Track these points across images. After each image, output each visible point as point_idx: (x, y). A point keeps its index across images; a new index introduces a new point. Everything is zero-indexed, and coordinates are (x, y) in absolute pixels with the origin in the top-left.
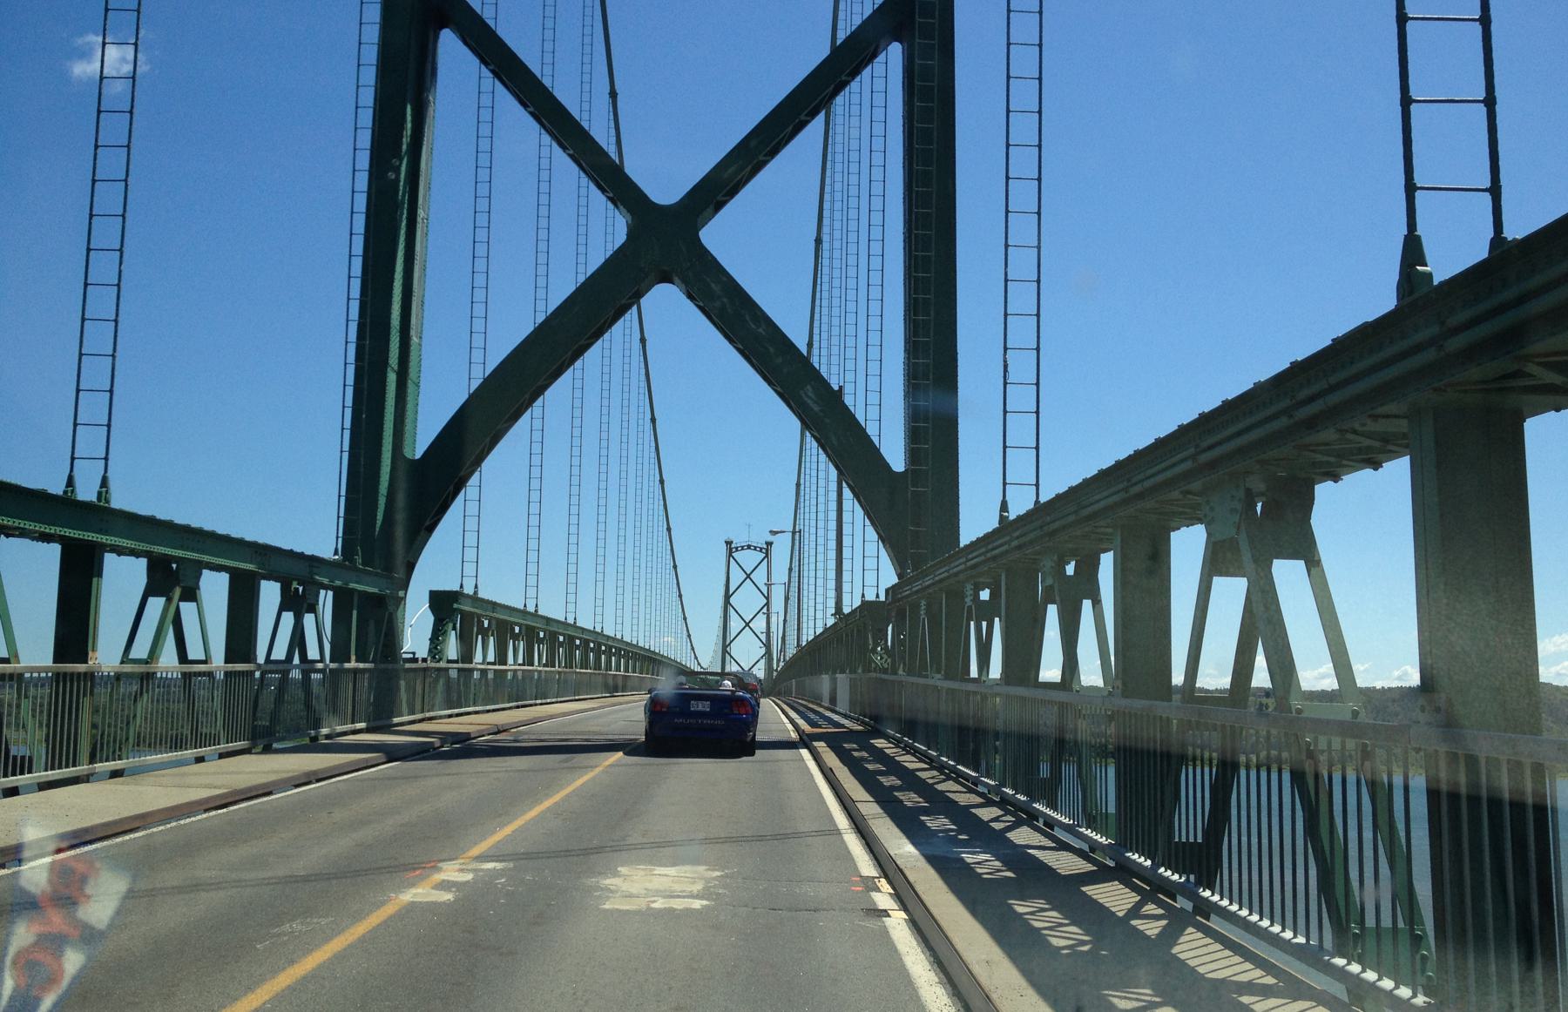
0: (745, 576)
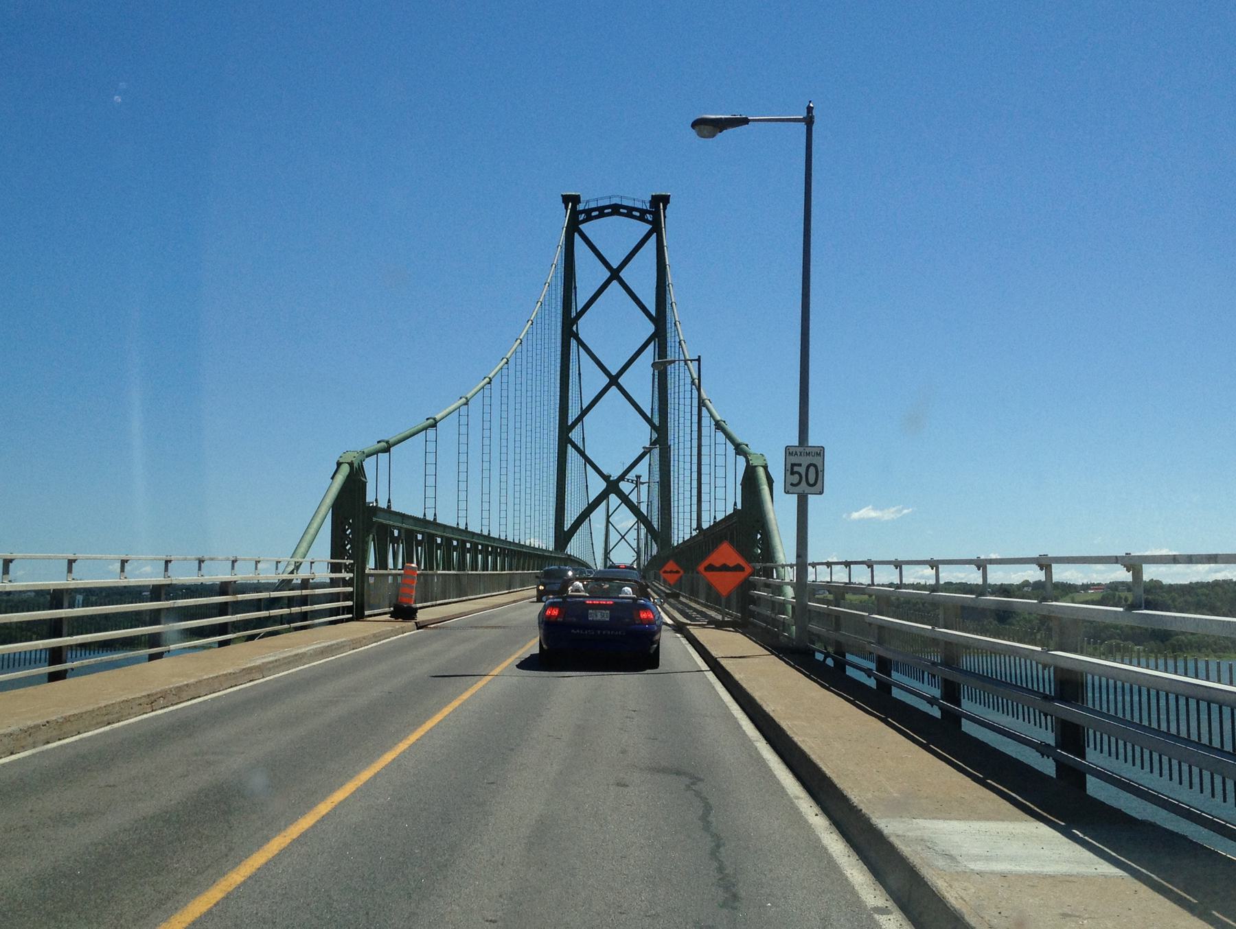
0: (625, 537)
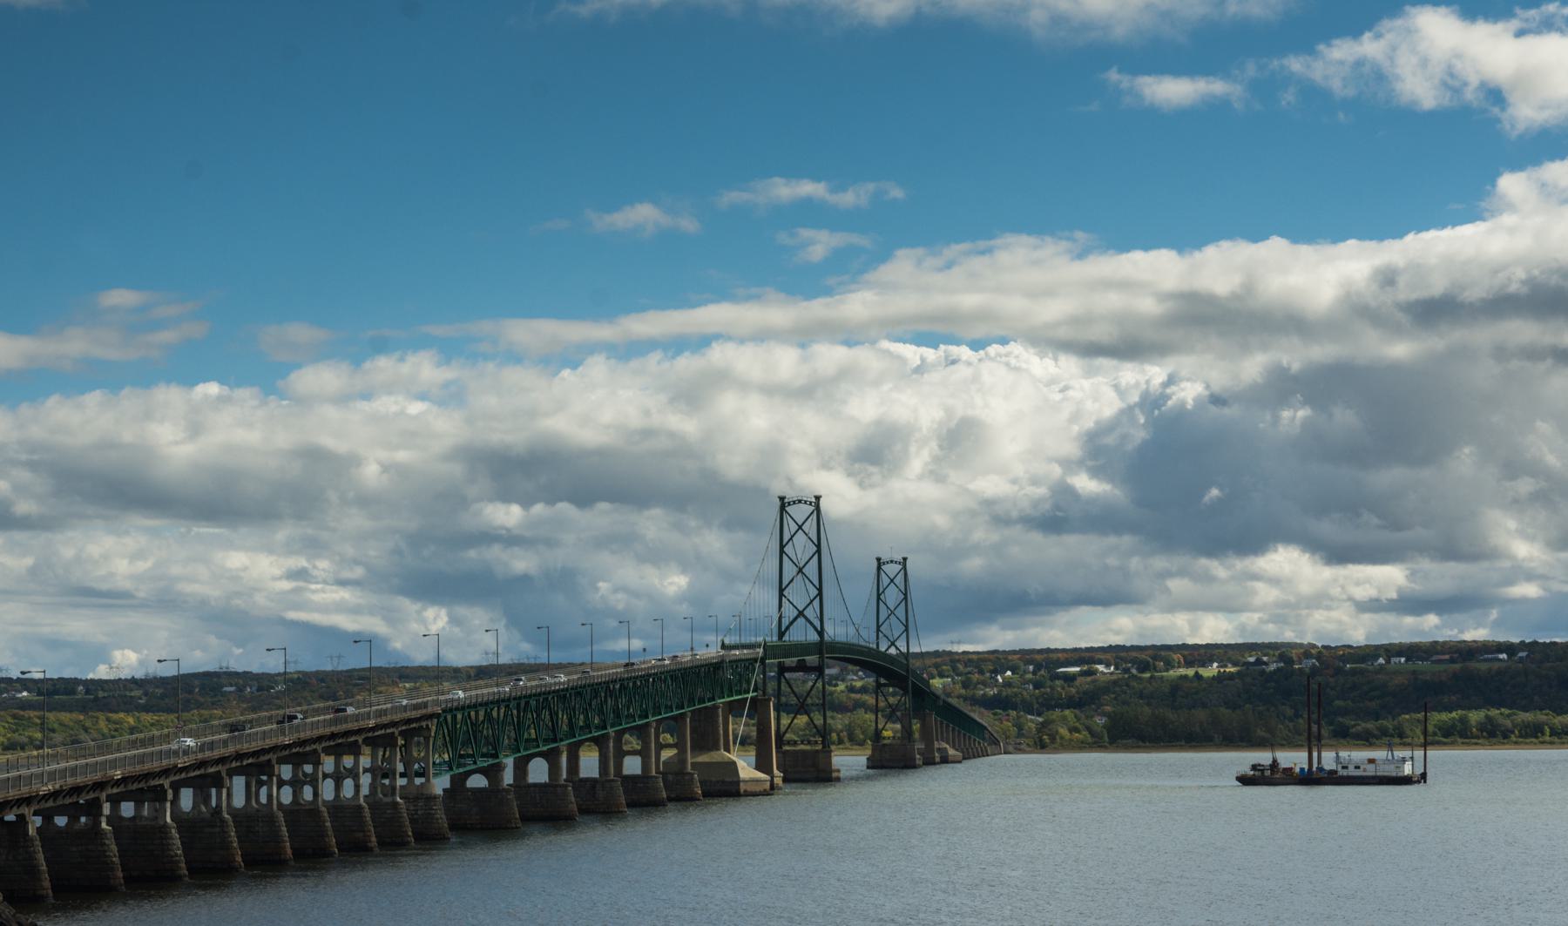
0: (797, 527)
